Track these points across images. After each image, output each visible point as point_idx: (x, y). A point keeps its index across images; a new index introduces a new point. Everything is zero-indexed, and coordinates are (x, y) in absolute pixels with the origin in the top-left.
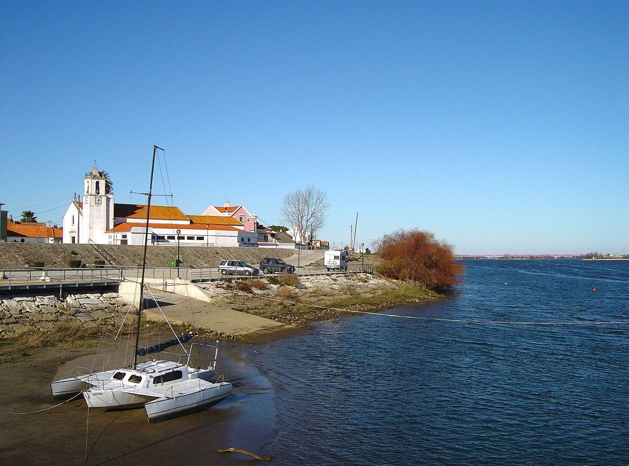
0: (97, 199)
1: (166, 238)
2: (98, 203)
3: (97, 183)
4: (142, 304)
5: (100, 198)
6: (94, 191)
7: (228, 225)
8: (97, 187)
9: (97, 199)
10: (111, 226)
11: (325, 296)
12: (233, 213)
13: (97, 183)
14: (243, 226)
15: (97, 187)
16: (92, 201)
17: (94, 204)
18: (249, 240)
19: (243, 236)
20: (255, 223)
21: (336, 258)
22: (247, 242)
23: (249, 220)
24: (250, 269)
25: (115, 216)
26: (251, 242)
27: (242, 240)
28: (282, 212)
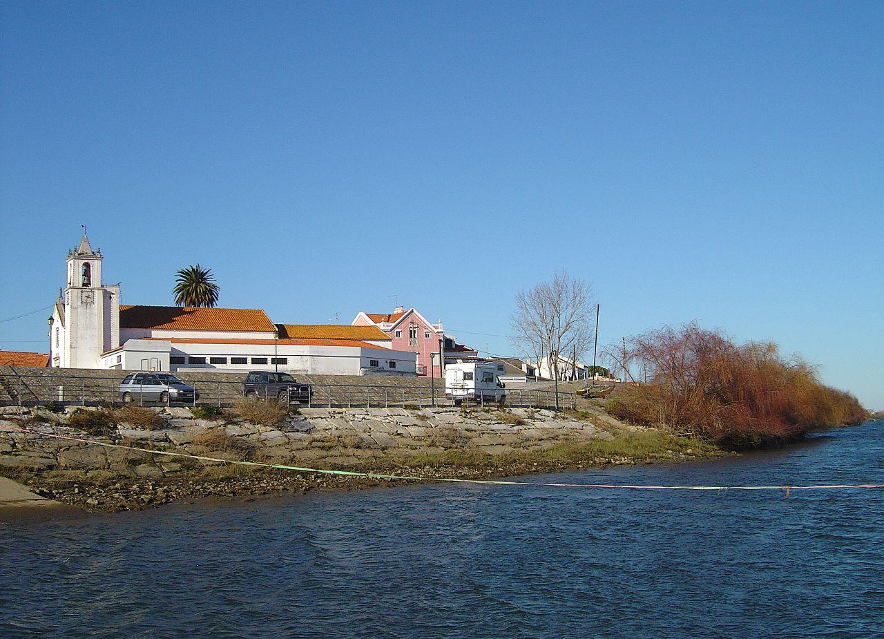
0: (85, 294)
1: (208, 361)
2: (87, 302)
3: (87, 266)
4: (23, 503)
5: (91, 294)
6: (80, 280)
7: (361, 340)
8: (87, 273)
9: (85, 294)
10: (115, 344)
11: (358, 447)
12: (397, 322)
13: (87, 266)
14: (390, 340)
15: (87, 273)
16: (75, 299)
17: (79, 303)
18: (392, 365)
19: (375, 356)
20: (440, 341)
21: (467, 376)
22: (387, 367)
23: (427, 336)
24: (173, 391)
25: (121, 326)
26: (398, 367)
27: (374, 363)
28: (515, 323)
